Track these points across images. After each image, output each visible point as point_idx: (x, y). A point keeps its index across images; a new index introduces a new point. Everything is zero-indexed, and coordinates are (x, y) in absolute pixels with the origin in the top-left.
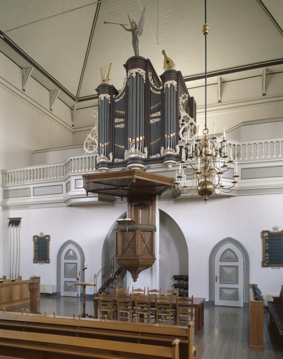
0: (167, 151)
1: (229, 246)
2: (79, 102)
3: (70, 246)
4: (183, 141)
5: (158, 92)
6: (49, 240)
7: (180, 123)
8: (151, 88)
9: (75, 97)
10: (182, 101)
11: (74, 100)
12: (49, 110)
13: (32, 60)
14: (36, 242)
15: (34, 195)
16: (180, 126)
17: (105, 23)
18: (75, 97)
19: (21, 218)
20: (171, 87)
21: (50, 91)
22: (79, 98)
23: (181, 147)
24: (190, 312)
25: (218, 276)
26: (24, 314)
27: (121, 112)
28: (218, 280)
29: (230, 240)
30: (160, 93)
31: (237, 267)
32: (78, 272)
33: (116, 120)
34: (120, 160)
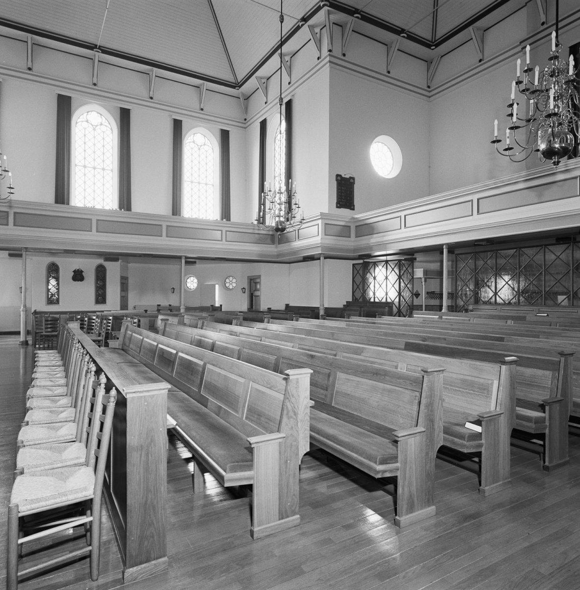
6: (354, 183)
9: (429, 41)
13: (418, 37)
14: (339, 183)
18: (429, 41)
21: (427, 62)
22: (437, 40)
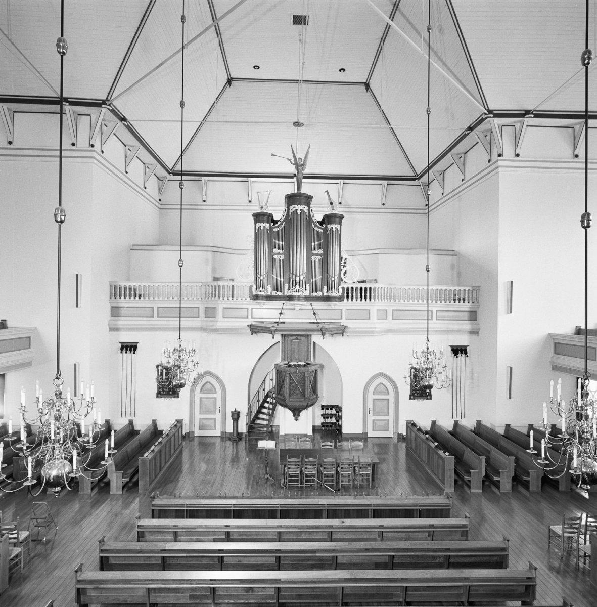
1: (381, 380)
2: (174, 175)
3: (208, 378)
8: (313, 224)
11: (169, 173)
12: (142, 187)
15: (158, 316)
16: (342, 267)
17: (272, 155)
19: (138, 343)
23: (343, 288)
24: (310, 435)
25: (371, 409)
26: (583, 514)
27: (280, 242)
28: (371, 412)
30: (322, 231)
31: (388, 400)
32: (218, 407)
33: (282, 257)
34: (280, 294)
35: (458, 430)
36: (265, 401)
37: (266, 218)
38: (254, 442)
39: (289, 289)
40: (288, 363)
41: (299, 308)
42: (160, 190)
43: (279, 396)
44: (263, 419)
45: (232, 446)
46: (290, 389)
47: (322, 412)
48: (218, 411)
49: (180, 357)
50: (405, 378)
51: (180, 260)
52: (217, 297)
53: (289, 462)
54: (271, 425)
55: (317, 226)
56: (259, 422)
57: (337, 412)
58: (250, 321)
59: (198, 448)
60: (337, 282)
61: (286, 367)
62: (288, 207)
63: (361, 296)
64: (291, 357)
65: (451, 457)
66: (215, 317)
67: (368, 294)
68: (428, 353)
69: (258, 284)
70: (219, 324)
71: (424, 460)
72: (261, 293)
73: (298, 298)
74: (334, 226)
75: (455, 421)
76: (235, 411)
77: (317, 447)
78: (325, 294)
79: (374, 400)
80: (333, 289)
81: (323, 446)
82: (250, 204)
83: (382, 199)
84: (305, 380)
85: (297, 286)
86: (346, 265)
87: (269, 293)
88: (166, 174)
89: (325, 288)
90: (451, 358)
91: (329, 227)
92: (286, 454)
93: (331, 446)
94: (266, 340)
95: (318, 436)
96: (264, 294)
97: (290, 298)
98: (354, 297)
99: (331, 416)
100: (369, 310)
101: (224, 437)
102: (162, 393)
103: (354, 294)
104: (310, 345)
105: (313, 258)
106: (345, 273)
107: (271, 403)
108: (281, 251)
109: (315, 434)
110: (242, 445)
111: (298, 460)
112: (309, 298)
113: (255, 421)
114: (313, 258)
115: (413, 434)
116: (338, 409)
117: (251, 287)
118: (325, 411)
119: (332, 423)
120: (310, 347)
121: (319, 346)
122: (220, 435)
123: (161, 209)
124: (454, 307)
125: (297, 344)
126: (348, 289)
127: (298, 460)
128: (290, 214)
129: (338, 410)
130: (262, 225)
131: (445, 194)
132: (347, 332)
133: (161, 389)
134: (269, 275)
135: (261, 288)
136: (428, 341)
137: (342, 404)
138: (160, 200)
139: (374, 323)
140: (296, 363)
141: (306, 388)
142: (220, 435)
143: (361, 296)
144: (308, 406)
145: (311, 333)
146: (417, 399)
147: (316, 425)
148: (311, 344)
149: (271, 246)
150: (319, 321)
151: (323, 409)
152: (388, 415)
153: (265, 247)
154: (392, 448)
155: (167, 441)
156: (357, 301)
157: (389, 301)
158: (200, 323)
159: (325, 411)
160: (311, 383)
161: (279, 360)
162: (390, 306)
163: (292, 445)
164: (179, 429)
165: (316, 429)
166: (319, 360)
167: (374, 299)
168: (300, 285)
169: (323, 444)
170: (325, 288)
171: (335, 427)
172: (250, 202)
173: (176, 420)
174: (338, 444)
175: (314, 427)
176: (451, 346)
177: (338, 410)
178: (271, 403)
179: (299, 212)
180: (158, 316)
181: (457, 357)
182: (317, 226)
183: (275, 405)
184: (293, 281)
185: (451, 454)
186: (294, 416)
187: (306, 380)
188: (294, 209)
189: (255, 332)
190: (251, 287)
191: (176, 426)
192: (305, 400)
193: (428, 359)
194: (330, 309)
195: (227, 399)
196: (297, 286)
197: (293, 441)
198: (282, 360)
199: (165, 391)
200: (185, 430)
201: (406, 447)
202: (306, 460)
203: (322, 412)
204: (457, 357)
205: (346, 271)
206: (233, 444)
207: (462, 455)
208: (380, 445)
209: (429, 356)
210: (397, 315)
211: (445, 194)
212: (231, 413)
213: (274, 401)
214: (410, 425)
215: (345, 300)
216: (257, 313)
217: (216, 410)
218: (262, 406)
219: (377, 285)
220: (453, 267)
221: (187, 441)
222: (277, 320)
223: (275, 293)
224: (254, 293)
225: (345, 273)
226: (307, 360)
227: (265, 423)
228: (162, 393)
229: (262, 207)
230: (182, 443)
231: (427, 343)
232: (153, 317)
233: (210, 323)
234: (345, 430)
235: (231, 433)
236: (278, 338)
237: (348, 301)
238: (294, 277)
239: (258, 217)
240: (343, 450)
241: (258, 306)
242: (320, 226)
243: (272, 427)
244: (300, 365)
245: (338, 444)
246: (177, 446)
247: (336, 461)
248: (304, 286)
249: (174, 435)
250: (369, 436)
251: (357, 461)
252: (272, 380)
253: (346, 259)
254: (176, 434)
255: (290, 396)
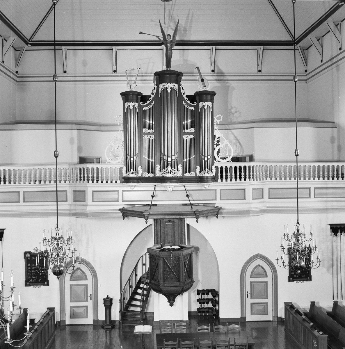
0: (205, 173)
4: (218, 161)
5: (191, 107)
7: (215, 143)
8: (184, 102)
10: (216, 122)
11: (27, 44)
15: (24, 202)
16: (215, 146)
17: (141, 33)
19: (4, 229)
20: (207, 108)
23: (217, 168)
25: (249, 292)
28: (249, 295)
29: (259, 256)
30: (193, 108)
32: (89, 295)
33: (153, 137)
34: (151, 175)
35: (338, 311)
36: (138, 287)
37: (135, 97)
38: (128, 330)
39: (160, 170)
40: (162, 246)
41: (171, 189)
42: (18, 61)
43: (153, 282)
44: (136, 306)
45: (104, 335)
46: (164, 274)
47: (197, 297)
48: (89, 298)
49: (58, 245)
50: (277, 260)
51: (56, 151)
52: (86, 180)
53: (166, 345)
54: (145, 311)
55: (187, 104)
56: (132, 309)
57: (214, 296)
58: (121, 205)
59: (70, 338)
60: (210, 162)
61: (160, 251)
62: (157, 85)
63: (236, 176)
64: (164, 241)
65: (324, 335)
66: (84, 201)
67: (243, 174)
68: (298, 236)
69: (130, 166)
70: (88, 208)
71: (301, 341)
72: (132, 175)
73: (171, 180)
74: (206, 104)
75: (334, 302)
76: (108, 298)
77: (193, 331)
78: (198, 174)
79: (251, 283)
80: (207, 169)
81: (200, 330)
82: (114, 74)
83: (258, 65)
84: (179, 264)
85: (169, 168)
86: (219, 143)
87: (140, 175)
88: (22, 44)
89: (198, 169)
90: (331, 237)
91: (201, 104)
92: (162, 338)
93: (207, 329)
94: (139, 224)
95: (194, 323)
96: (135, 176)
97: (162, 180)
98: (229, 177)
99: (208, 301)
100: (244, 190)
101: (97, 325)
102: (31, 281)
103: (229, 174)
104: (183, 227)
105: (185, 137)
106: (218, 152)
107: (145, 289)
108: (151, 131)
109: (192, 320)
110: (116, 333)
111: (175, 343)
112: (181, 179)
113: (128, 308)
114: (185, 137)
115: (291, 316)
116: (215, 293)
117: (121, 169)
118: (201, 296)
119: (209, 308)
120: (183, 230)
121: (191, 226)
122: (92, 323)
123: (17, 82)
124: (332, 184)
125: (170, 227)
126: (222, 168)
127: (175, 343)
128: (160, 92)
129: (215, 295)
130: (131, 104)
131: (324, 61)
132: (222, 213)
133: (29, 277)
134: (139, 156)
135: (132, 170)
136: (298, 223)
137: (219, 288)
138: (17, 72)
139: (250, 203)
140: (170, 247)
141: (181, 272)
142: (92, 323)
143: (236, 176)
144: (181, 292)
145: (184, 217)
146: (297, 281)
147: (192, 310)
148: (185, 226)
149: (141, 125)
150: (192, 202)
151: (198, 294)
152: (267, 297)
153: (134, 122)
154: (271, 332)
155: (42, 329)
156: (231, 180)
157: (265, 179)
158: (68, 207)
159: (201, 296)
160: (185, 266)
161: (151, 244)
162: (266, 185)
163: (169, 331)
164: (51, 317)
165: (192, 314)
166: (193, 243)
167: (250, 178)
168: (171, 167)
169: (199, 328)
170: (198, 169)
171: (212, 312)
172: (115, 71)
173: (48, 308)
174: (215, 327)
175: (190, 313)
176: (330, 225)
177: (215, 295)
178: (145, 289)
179: (169, 90)
180: (24, 202)
181: (337, 236)
182: (187, 104)
183: (148, 291)
184: (164, 162)
185: (324, 333)
186: (169, 301)
187: (181, 263)
188: (164, 88)
189: (127, 216)
190: (121, 169)
191: (48, 314)
192: (180, 284)
193: (298, 241)
194: (204, 190)
195: (99, 285)
196: (169, 168)
197: (168, 326)
198: (155, 244)
199: (34, 279)
200: (57, 318)
201: (285, 330)
202: (183, 343)
203: (197, 297)
204: (337, 236)
205: (219, 150)
206: (106, 332)
207: (338, 335)
208: (258, 330)
209: (300, 239)
210: (274, 194)
211: (324, 61)
212: (103, 301)
213: (148, 287)
214: (288, 307)
215: (219, 180)
216: (129, 196)
217: (87, 296)
218: (135, 293)
219: (252, 164)
220: (332, 140)
221: (59, 330)
222: (150, 203)
223: (146, 175)
224: (125, 175)
225: (218, 152)
226: (181, 243)
227: (139, 309)
228: (31, 281)
229: (131, 86)
230: (54, 331)
231: (298, 225)
232: (19, 202)
233: (79, 207)
234: (223, 315)
235: (103, 321)
236: (151, 221)
237: (222, 181)
238: (165, 158)
239: (127, 96)
240: (219, 334)
241: (129, 189)
242: (191, 104)
243: (146, 314)
244: (174, 249)
245: (215, 327)
246: (50, 335)
247: (212, 343)
248: (176, 167)
249: (48, 323)
250: (247, 320)
251: (233, 343)
252: (144, 265)
253: (219, 138)
254: (50, 323)
255: (164, 281)
